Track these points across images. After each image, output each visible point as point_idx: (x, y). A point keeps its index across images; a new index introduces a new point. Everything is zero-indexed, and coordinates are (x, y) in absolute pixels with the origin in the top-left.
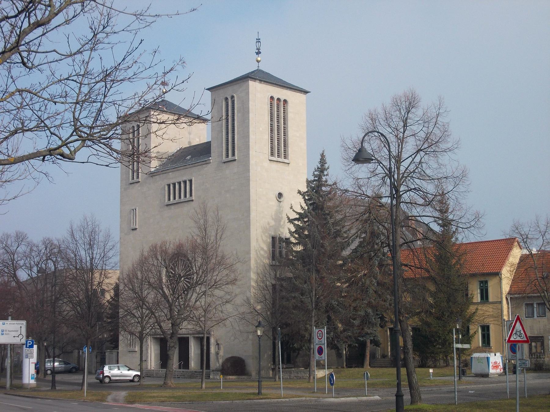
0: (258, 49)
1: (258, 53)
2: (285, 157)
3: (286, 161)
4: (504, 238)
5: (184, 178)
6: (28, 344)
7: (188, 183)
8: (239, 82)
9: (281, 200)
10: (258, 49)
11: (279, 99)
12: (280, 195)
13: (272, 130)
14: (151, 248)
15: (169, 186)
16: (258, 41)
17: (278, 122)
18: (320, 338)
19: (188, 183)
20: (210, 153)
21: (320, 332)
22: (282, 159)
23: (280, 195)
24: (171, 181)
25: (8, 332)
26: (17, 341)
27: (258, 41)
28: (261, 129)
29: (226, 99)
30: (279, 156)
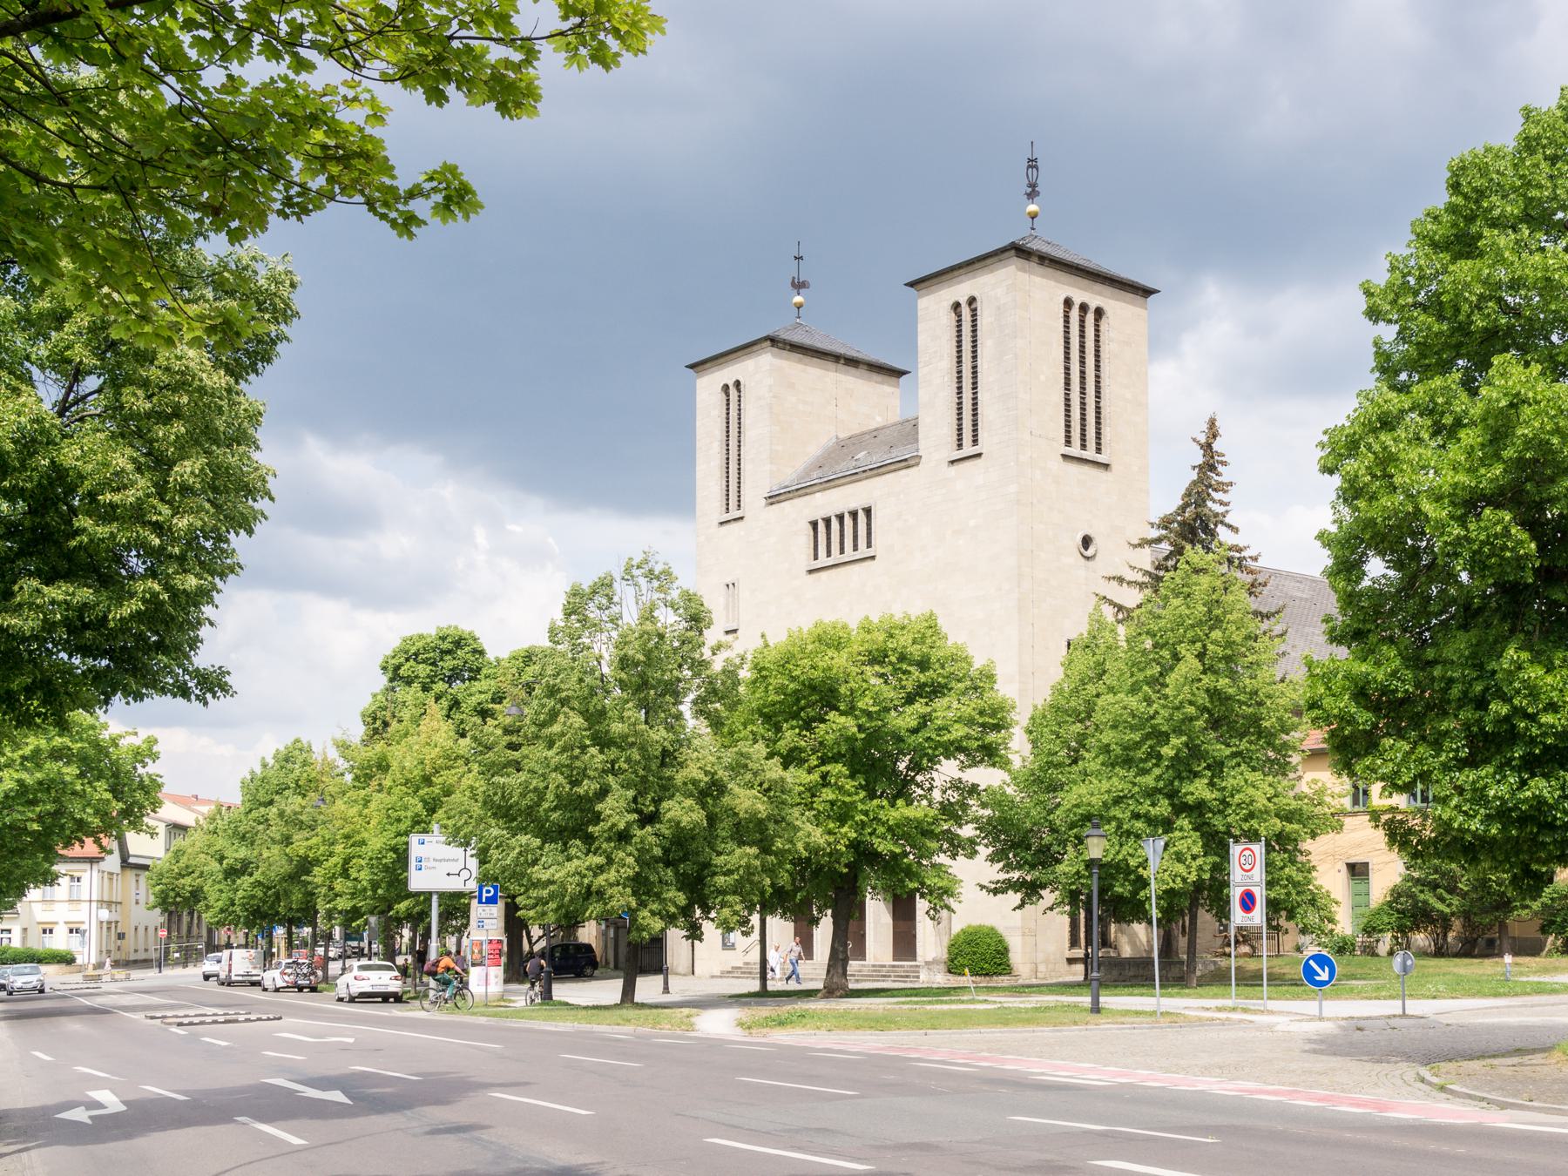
0: (1033, 186)
1: (1032, 193)
2: (1099, 450)
3: (1100, 458)
4: (426, 1109)
5: (852, 506)
6: (485, 895)
7: (862, 517)
8: (989, 261)
9: (1089, 553)
10: (1033, 186)
11: (1084, 308)
12: (1087, 541)
13: (1067, 383)
14: (951, 902)
15: (814, 524)
16: (1032, 164)
17: (1082, 362)
18: (1247, 867)
19: (862, 517)
20: (917, 440)
21: (1247, 853)
22: (1090, 454)
23: (1087, 541)
24: (818, 515)
25: (432, 864)
26: (455, 885)
27: (1032, 164)
28: (1042, 378)
29: (957, 306)
30: (1083, 447)
